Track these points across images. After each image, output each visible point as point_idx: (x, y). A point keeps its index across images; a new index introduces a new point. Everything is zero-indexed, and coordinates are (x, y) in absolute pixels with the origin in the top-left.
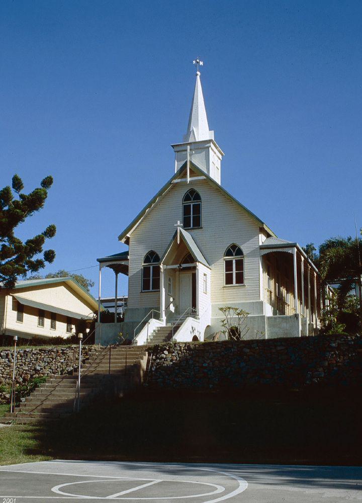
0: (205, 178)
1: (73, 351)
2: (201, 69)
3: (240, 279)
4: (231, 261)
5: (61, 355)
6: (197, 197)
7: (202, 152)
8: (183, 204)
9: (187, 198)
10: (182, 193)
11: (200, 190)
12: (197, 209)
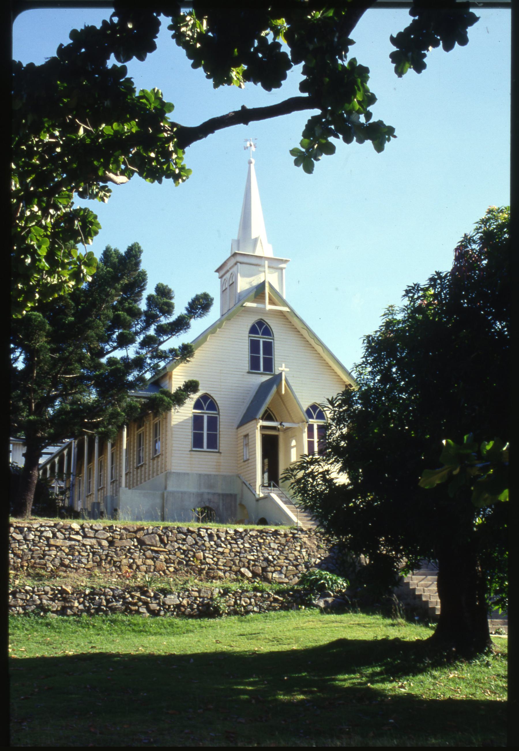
0: (289, 310)
1: (307, 536)
2: (75, 117)
3: (213, 443)
4: (202, 417)
5: (292, 540)
6: (267, 332)
7: (275, 272)
8: (249, 337)
9: (253, 330)
10: (250, 321)
11: (274, 324)
12: (269, 348)
